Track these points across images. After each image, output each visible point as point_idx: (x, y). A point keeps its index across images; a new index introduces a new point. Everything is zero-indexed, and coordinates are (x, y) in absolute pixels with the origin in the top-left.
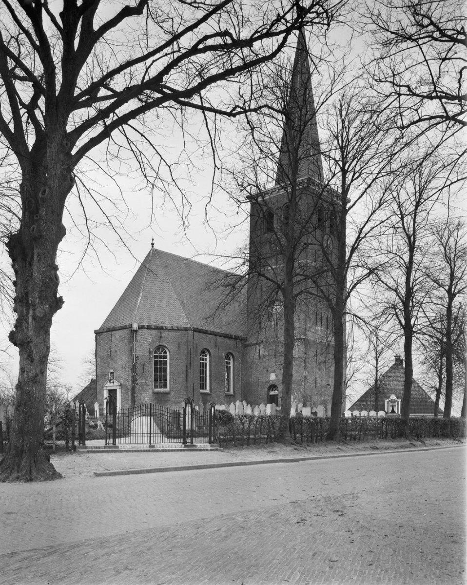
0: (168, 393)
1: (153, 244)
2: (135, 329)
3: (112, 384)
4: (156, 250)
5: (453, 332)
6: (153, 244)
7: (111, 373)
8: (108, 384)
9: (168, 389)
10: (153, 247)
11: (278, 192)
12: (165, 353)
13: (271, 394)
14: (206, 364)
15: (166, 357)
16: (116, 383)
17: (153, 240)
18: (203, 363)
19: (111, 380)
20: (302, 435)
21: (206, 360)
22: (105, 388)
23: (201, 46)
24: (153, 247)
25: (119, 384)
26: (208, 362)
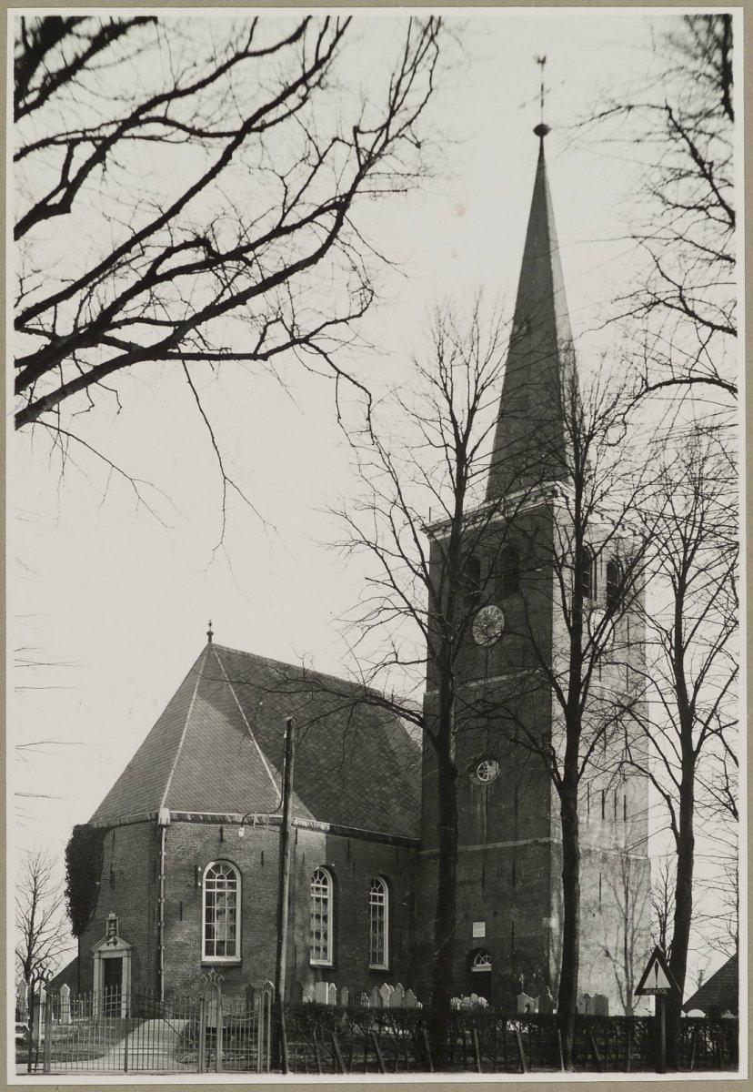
0: (237, 966)
1: (210, 634)
2: (164, 822)
3: (112, 947)
4: (220, 650)
5: (619, 701)
6: (210, 634)
7: (111, 921)
8: (104, 947)
9: (236, 959)
10: (210, 640)
11: (535, 501)
12: (232, 876)
13: (474, 970)
14: (381, 908)
15: (233, 885)
16: (121, 944)
17: (210, 624)
18: (375, 906)
19: (110, 937)
20: (351, 1055)
21: (381, 899)
22: (96, 955)
23: (142, 117)
24: (210, 640)
25: (128, 946)
26: (386, 903)
